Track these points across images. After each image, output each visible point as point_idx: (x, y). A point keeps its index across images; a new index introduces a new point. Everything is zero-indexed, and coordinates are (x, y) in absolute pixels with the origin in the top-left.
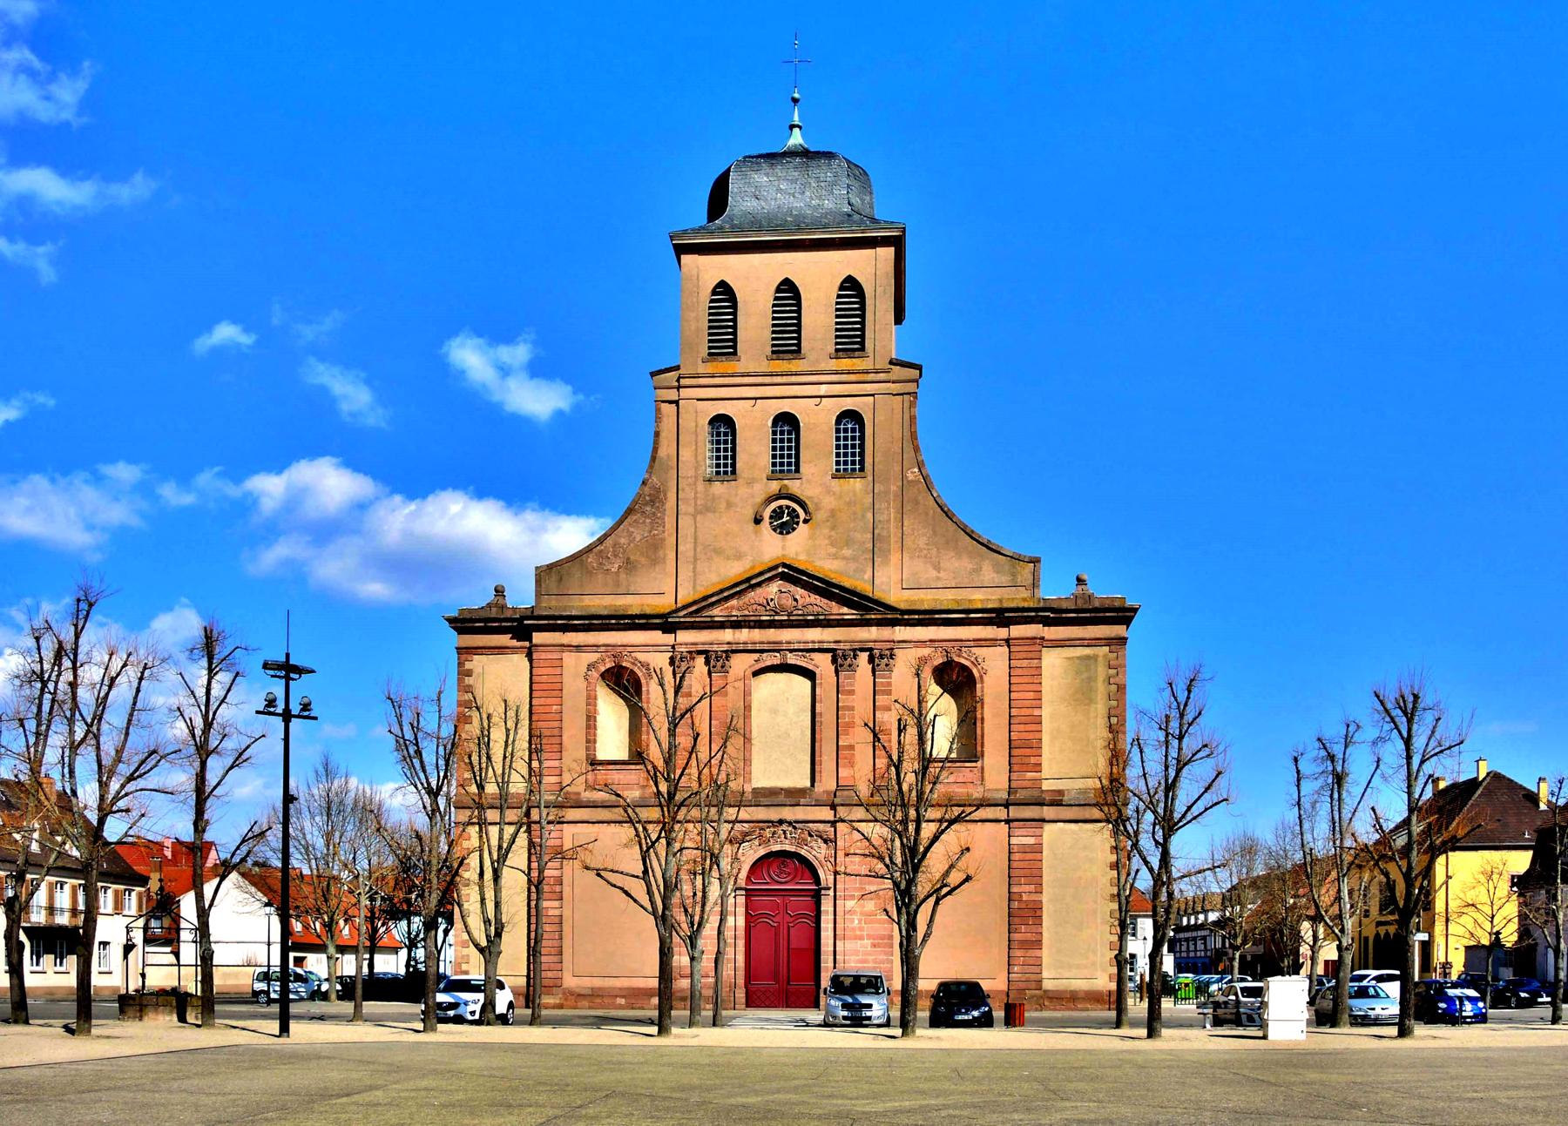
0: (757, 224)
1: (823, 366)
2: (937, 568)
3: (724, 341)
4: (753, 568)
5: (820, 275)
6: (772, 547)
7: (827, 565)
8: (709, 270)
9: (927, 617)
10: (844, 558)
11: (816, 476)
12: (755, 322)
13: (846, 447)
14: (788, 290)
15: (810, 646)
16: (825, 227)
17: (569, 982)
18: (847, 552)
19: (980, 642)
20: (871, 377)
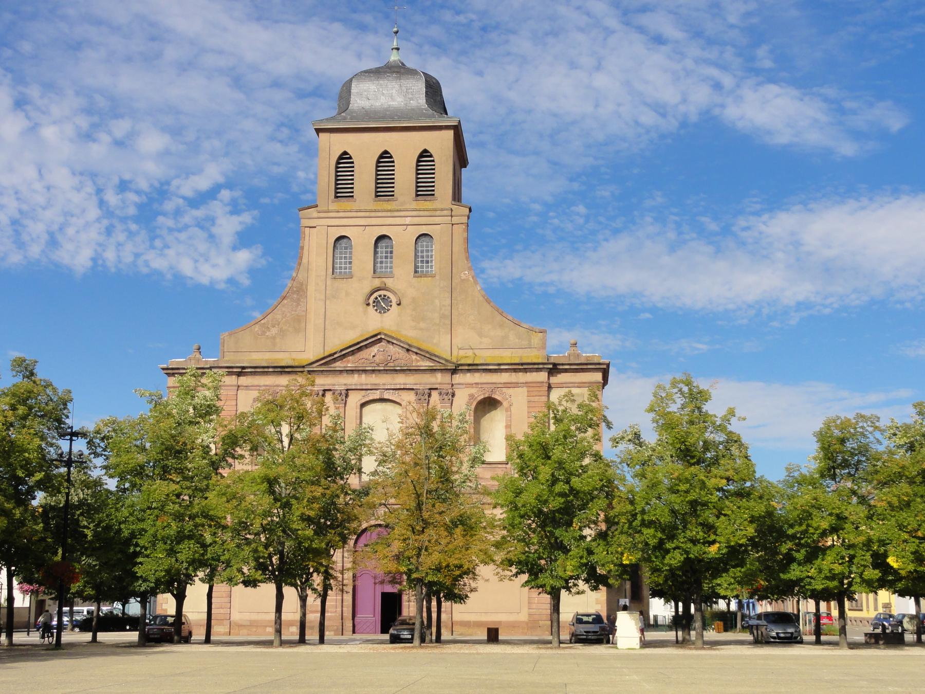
0: (368, 114)
1: (407, 207)
2: (481, 335)
3: (342, 189)
4: (361, 335)
5: (405, 148)
6: (374, 322)
7: (409, 333)
8: (338, 143)
9: (473, 368)
10: (421, 329)
11: (401, 278)
12: (364, 176)
13: (345, 263)
14: (385, 156)
15: (398, 387)
16: (410, 119)
17: (236, 616)
18: (422, 325)
19: (508, 385)
20: (438, 213)
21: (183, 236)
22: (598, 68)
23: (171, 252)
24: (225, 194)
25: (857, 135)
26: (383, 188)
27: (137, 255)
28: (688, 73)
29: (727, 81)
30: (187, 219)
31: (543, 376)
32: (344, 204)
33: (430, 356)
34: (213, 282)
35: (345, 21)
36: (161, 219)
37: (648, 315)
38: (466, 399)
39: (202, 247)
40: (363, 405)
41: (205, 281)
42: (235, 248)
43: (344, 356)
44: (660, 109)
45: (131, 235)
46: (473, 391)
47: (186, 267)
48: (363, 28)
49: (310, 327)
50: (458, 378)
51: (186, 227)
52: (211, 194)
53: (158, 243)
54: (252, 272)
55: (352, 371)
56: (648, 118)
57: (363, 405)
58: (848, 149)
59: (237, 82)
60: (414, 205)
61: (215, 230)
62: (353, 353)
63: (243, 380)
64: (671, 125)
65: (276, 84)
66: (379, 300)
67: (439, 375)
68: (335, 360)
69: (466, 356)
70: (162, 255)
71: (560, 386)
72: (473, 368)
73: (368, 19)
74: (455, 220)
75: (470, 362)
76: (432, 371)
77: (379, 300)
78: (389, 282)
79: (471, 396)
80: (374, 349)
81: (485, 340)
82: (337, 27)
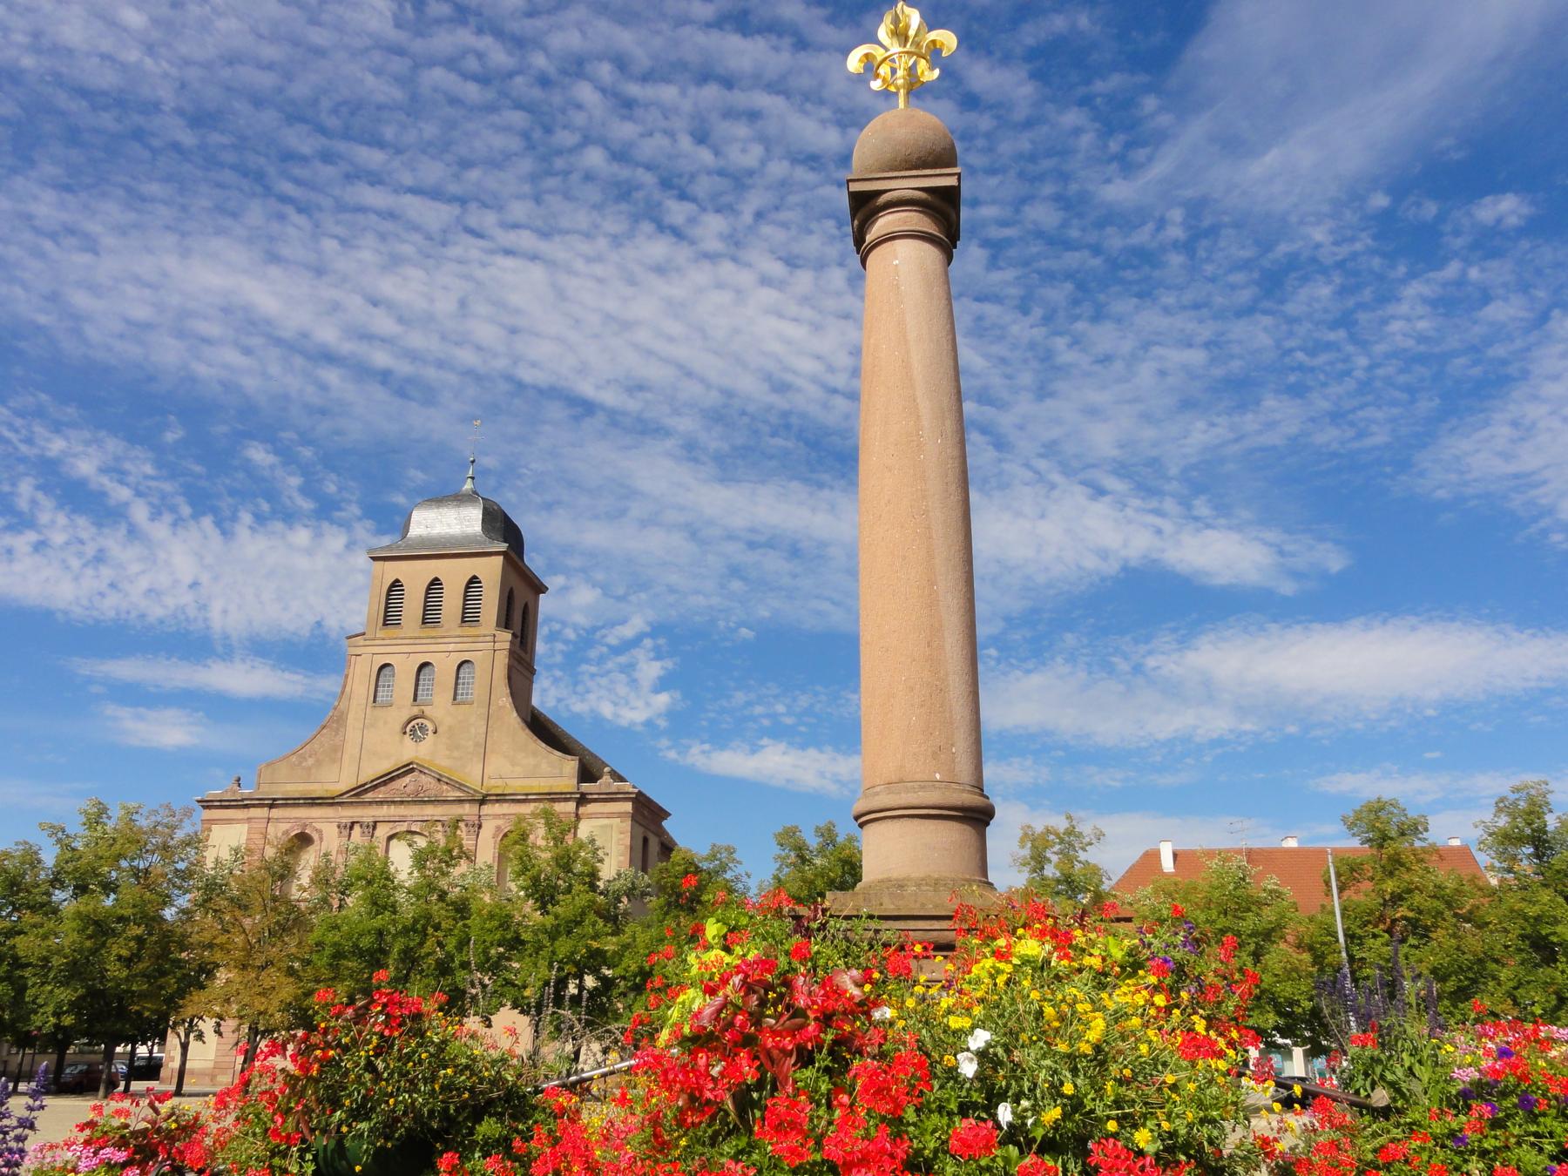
0: (424, 542)
5: (454, 574)
6: (409, 751)
9: (501, 798)
11: (439, 706)
18: (456, 754)
21: (604, 681)
22: (1042, 516)
23: (592, 697)
24: (648, 642)
25: (1296, 575)
26: (429, 616)
27: (559, 700)
28: (1130, 522)
29: (1167, 526)
30: (610, 665)
31: (571, 806)
32: (391, 631)
33: (460, 786)
34: (633, 724)
35: (806, 481)
36: (584, 667)
37: (1061, 753)
38: (493, 831)
39: (622, 690)
40: (390, 838)
41: (624, 723)
42: (657, 690)
43: (376, 787)
44: (1104, 554)
45: (556, 680)
46: (500, 822)
47: (607, 710)
48: (821, 485)
49: (346, 757)
50: (486, 809)
51: (609, 672)
52: (636, 642)
53: (580, 688)
54: (671, 714)
55: (381, 803)
56: (1091, 563)
57: (390, 838)
58: (1288, 588)
59: (693, 533)
60: (459, 632)
61: (636, 675)
62: (385, 783)
63: (275, 813)
64: (1112, 568)
65: (731, 537)
66: (414, 728)
67: (467, 806)
68: (366, 791)
69: (494, 786)
70: (582, 701)
71: (590, 816)
72: (501, 798)
73: (826, 477)
74: (497, 646)
75: (499, 791)
76: (460, 801)
77: (414, 728)
78: (428, 710)
79: (498, 828)
80: (407, 779)
81: (518, 769)
82: (795, 485)
